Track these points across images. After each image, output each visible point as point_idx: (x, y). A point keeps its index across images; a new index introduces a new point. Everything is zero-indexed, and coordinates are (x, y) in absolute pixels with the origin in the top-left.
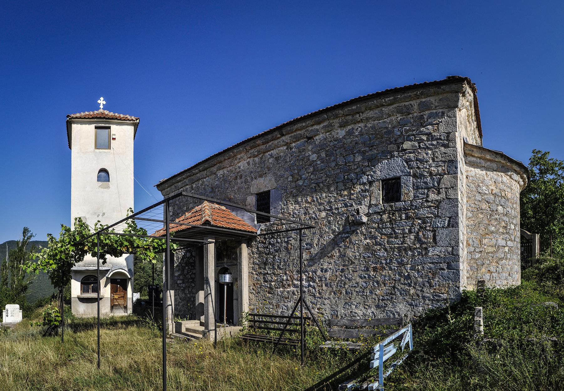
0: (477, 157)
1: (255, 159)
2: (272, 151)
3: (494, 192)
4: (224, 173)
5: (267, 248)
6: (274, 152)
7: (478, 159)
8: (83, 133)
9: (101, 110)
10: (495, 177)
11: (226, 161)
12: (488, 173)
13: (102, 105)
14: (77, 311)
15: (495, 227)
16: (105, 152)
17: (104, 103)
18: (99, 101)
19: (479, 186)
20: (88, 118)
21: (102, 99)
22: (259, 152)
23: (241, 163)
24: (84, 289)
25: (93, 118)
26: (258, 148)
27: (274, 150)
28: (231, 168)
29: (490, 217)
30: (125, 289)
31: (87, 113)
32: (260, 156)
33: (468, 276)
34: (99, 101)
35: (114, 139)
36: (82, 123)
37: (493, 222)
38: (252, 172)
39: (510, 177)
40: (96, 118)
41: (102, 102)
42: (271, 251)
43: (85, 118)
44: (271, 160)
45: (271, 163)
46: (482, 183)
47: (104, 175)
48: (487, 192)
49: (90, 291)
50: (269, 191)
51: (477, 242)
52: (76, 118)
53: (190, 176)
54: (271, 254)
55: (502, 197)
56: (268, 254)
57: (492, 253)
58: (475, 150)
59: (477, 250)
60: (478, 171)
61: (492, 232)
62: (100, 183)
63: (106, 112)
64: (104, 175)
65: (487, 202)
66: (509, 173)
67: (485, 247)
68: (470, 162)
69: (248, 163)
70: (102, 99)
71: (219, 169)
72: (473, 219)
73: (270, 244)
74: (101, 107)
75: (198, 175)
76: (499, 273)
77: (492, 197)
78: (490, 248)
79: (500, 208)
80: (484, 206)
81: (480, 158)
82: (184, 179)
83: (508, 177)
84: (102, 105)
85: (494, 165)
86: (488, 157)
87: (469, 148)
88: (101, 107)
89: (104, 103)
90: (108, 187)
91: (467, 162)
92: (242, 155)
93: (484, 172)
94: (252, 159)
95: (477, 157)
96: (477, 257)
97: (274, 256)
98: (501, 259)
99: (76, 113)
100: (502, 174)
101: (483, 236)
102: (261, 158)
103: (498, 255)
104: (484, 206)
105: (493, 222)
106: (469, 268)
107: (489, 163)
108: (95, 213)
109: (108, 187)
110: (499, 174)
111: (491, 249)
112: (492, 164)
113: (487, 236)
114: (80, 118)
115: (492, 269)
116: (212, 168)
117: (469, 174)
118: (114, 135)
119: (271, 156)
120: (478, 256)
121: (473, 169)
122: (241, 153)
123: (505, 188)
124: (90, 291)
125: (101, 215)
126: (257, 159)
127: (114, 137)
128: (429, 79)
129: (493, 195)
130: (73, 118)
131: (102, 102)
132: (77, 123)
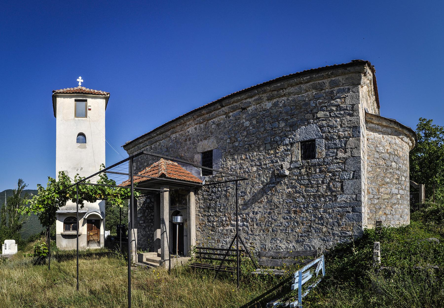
0: (375, 124)
1: (201, 125)
2: (214, 119)
3: (389, 151)
4: (176, 136)
5: (210, 195)
6: (216, 120)
7: (377, 125)
8: (66, 105)
9: (80, 87)
10: (390, 139)
11: (178, 127)
12: (384, 136)
13: (80, 82)
14: (61, 245)
15: (390, 179)
16: (82, 120)
17: (82, 81)
18: (78, 80)
19: (377, 146)
20: (70, 93)
21: (80, 78)
22: (204, 120)
23: (190, 128)
24: (66, 228)
25: (73, 93)
26: (203, 116)
27: (216, 119)
28: (182, 132)
29: (386, 171)
30: (99, 228)
31: (68, 89)
32: (205, 123)
33: (369, 217)
34: (78, 80)
35: (90, 109)
36: (64, 97)
37: (388, 175)
38: (198, 136)
39: (402, 139)
40: (76, 93)
41: (80, 80)
42: (214, 197)
43: (67, 93)
44: (213, 126)
45: (214, 128)
46: (379, 144)
47: (82, 138)
48: (383, 151)
49: (71, 229)
50: (212, 151)
51: (375, 191)
52: (60, 93)
53: (149, 139)
54: (213, 200)
55: (395, 155)
56: (211, 200)
57: (387, 199)
58: (374, 118)
59: (376, 197)
60: (376, 135)
61: (388, 183)
62: (79, 144)
63: (84, 88)
64: (82, 138)
65: (384, 159)
66: (401, 137)
67: (382, 195)
68: (370, 127)
69: (196, 129)
70: (80, 78)
71: (173, 133)
72: (373, 172)
73: (212, 192)
74: (80, 84)
75: (156, 138)
76: (393, 215)
77: (387, 155)
78: (386, 195)
79: (394, 164)
80: (381, 162)
81: (378, 125)
82: (145, 141)
83: (400, 140)
84: (80, 82)
85: (389, 130)
86: (384, 124)
87: (369, 116)
88: (80, 84)
89: (82, 81)
90: (85, 147)
91: (368, 127)
92: (190, 122)
93: (381, 136)
94: (198, 125)
95: (375, 124)
96: (375, 202)
97: (216, 202)
98: (395, 204)
99: (60, 89)
100: (396, 137)
101: (380, 186)
102: (206, 125)
103: (392, 201)
104: (381, 162)
105: (388, 175)
106: (369, 211)
107: (385, 129)
108: (75, 168)
109: (85, 147)
110: (393, 137)
111: (386, 196)
112: (388, 129)
113: (384, 186)
114: (63, 93)
115: (387, 212)
116: (167, 132)
117: (370, 137)
118: (90, 106)
119: (214, 123)
120: (376, 201)
121: (372, 133)
122: (190, 120)
123: (397, 148)
124: (71, 229)
125: (79, 169)
126: (202, 125)
127: (90, 108)
128: (338, 62)
129: (388, 153)
130: (57, 93)
131: (80, 80)
132: (61, 97)
